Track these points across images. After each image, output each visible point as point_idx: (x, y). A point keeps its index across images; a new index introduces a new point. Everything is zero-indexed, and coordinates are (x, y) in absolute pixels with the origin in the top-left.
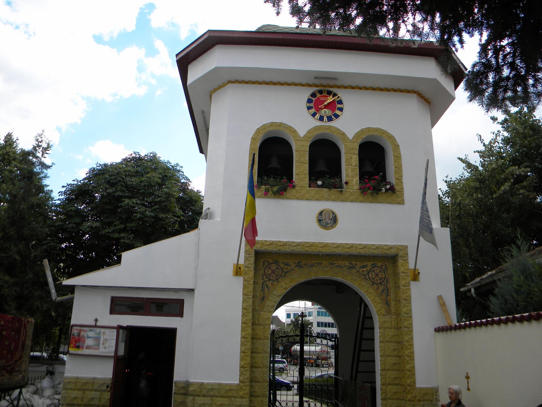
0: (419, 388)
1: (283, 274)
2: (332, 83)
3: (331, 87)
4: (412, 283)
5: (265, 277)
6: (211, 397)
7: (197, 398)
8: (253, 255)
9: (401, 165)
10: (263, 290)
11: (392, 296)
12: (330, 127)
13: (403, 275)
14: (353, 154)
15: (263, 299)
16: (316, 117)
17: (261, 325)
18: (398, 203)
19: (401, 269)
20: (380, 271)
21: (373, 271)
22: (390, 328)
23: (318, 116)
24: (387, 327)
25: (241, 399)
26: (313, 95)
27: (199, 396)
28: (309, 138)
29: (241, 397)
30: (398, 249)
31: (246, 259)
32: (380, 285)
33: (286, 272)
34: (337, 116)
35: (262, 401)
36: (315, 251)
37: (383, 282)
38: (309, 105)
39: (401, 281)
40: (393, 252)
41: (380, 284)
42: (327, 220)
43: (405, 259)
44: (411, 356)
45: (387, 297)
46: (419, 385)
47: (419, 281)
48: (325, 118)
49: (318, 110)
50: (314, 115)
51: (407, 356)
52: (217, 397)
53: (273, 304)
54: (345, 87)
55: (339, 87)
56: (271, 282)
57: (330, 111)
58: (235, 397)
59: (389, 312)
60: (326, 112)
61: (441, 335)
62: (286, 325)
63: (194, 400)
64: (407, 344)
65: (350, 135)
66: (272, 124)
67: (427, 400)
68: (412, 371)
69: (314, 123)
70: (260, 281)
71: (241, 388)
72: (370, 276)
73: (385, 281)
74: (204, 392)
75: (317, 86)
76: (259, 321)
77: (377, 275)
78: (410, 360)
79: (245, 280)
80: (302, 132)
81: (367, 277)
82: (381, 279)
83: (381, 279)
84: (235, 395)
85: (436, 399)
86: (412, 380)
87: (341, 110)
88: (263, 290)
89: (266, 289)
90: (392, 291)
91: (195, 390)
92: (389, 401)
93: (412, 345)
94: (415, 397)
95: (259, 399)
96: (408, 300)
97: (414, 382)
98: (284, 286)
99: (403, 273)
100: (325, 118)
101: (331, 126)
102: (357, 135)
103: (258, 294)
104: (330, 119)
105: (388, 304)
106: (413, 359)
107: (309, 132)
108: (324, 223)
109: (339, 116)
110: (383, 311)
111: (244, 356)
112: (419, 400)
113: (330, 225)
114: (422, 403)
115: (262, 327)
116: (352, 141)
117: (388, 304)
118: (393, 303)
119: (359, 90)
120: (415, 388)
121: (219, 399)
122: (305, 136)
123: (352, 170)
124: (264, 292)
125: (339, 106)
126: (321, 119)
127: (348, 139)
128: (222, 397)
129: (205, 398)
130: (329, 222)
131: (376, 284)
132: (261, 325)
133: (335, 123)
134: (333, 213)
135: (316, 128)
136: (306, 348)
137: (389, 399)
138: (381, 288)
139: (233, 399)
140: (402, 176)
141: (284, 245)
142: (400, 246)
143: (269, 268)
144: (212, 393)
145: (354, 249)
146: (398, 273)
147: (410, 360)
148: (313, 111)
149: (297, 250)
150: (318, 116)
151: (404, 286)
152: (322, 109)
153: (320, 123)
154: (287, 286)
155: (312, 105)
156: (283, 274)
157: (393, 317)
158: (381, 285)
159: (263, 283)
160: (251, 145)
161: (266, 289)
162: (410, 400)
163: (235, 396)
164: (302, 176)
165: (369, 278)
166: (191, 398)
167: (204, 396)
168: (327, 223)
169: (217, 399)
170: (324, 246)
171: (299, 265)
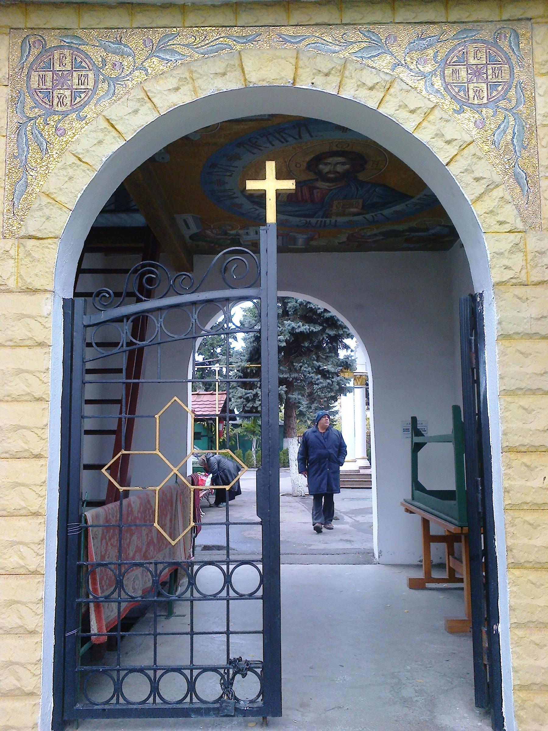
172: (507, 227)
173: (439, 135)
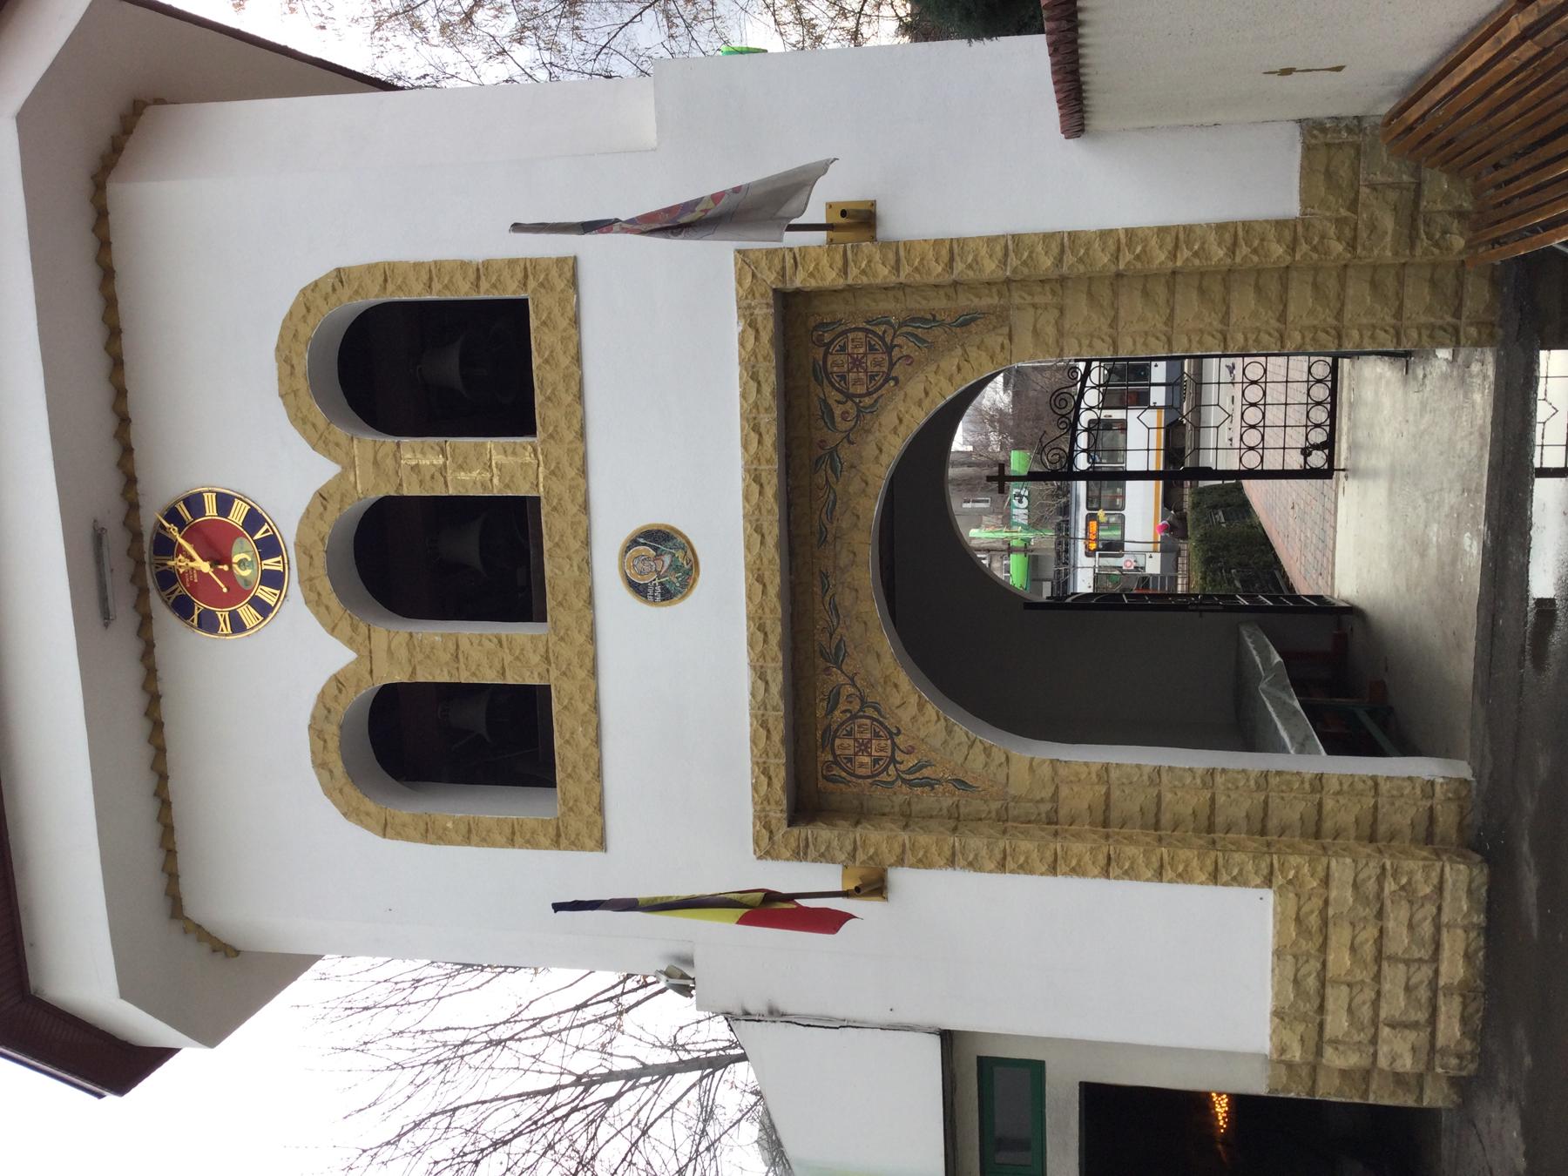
0: (1304, 203)
1: (870, 712)
2: (117, 539)
3: (137, 536)
4: (882, 232)
5: (884, 777)
6: (1323, 985)
7: (1329, 1032)
8: (807, 831)
10: (929, 783)
11: (939, 303)
13: (853, 271)
14: (397, 458)
15: (960, 783)
16: (271, 601)
17: (1055, 796)
18: (574, 282)
19: (831, 278)
20: (843, 348)
21: (843, 377)
22: (1062, 311)
23: (266, 594)
24: (1058, 325)
25: (1333, 884)
26: (183, 608)
27: (1321, 1026)
28: (354, 628)
29: (1326, 881)
30: (752, 292)
31: (825, 857)
32: (896, 353)
33: (862, 699)
34: (254, 520)
36: (779, 615)
37: (882, 339)
38: (225, 627)
39: (879, 281)
40: (765, 314)
41: (889, 349)
42: (663, 563)
43: (789, 262)
44: (1178, 236)
45: (942, 324)
46: (1289, 205)
47: (873, 204)
48: (271, 564)
49: (238, 592)
51: (1173, 256)
52: (1324, 964)
53: (978, 748)
54: (130, 481)
55: (133, 507)
56: (899, 756)
57: (236, 547)
58: (1326, 902)
59: (1001, 318)
60: (244, 560)
61: (1095, 122)
62: (1221, 1108)
63: (1335, 1042)
64: (1126, 257)
65: (323, 470)
66: (320, 765)
67: (1356, 174)
68: (1233, 233)
69: (294, 608)
70: (902, 794)
71: (1290, 882)
72: (861, 390)
73: (880, 330)
74: (1309, 1007)
75: (143, 593)
76: (1042, 800)
77: (857, 363)
78: (1189, 245)
79: (900, 862)
80: (337, 655)
81: (867, 401)
82: (872, 349)
83: (872, 349)
84: (1317, 903)
85: (1349, 130)
86: (1272, 234)
87: (225, 502)
88: (929, 783)
89: (926, 772)
90: (916, 304)
92: (1347, 316)
93: (1130, 233)
94: (1340, 222)
95: (1329, 804)
96: (952, 249)
97: (1280, 224)
98: (912, 709)
99: (845, 271)
100: (271, 564)
101: (299, 545)
102: (321, 444)
103: (947, 802)
104: (270, 547)
105: (967, 321)
106: (1188, 229)
107: (332, 630)
108: (674, 579)
109: (270, 609)
110: (995, 340)
111: (1174, 868)
113: (679, 554)
114: (1364, 191)
115: (1064, 791)
116: (349, 465)
117: (967, 321)
118: (966, 301)
119: (126, 340)
121: (1331, 957)
122: (350, 643)
123: (461, 468)
124: (939, 781)
125: (211, 510)
127: (341, 477)
128: (1324, 947)
129: (1330, 1005)
130: (667, 559)
131: (892, 365)
132: (1055, 796)
133: (286, 522)
134: (633, 542)
135: (315, 602)
136: (1081, 487)
137: (1339, 315)
138: (908, 348)
139: (1331, 912)
140: (463, 265)
141: (764, 724)
142: (739, 282)
143: (850, 760)
144: (1311, 983)
145: (764, 466)
147: (1189, 245)
148: (247, 614)
150: (266, 594)
152: (229, 577)
154: (914, 699)
155: (222, 614)
156: (870, 712)
157: (1016, 300)
158: (893, 347)
159: (904, 781)
161: (926, 772)
162: (1352, 245)
163: (1321, 903)
164: (508, 658)
165: (869, 394)
166: (1329, 1052)
167: (1321, 1009)
168: (675, 567)
169: (1330, 965)
170: (760, 579)
171: (836, 657)
172: (1006, 342)
173: (920, 404)
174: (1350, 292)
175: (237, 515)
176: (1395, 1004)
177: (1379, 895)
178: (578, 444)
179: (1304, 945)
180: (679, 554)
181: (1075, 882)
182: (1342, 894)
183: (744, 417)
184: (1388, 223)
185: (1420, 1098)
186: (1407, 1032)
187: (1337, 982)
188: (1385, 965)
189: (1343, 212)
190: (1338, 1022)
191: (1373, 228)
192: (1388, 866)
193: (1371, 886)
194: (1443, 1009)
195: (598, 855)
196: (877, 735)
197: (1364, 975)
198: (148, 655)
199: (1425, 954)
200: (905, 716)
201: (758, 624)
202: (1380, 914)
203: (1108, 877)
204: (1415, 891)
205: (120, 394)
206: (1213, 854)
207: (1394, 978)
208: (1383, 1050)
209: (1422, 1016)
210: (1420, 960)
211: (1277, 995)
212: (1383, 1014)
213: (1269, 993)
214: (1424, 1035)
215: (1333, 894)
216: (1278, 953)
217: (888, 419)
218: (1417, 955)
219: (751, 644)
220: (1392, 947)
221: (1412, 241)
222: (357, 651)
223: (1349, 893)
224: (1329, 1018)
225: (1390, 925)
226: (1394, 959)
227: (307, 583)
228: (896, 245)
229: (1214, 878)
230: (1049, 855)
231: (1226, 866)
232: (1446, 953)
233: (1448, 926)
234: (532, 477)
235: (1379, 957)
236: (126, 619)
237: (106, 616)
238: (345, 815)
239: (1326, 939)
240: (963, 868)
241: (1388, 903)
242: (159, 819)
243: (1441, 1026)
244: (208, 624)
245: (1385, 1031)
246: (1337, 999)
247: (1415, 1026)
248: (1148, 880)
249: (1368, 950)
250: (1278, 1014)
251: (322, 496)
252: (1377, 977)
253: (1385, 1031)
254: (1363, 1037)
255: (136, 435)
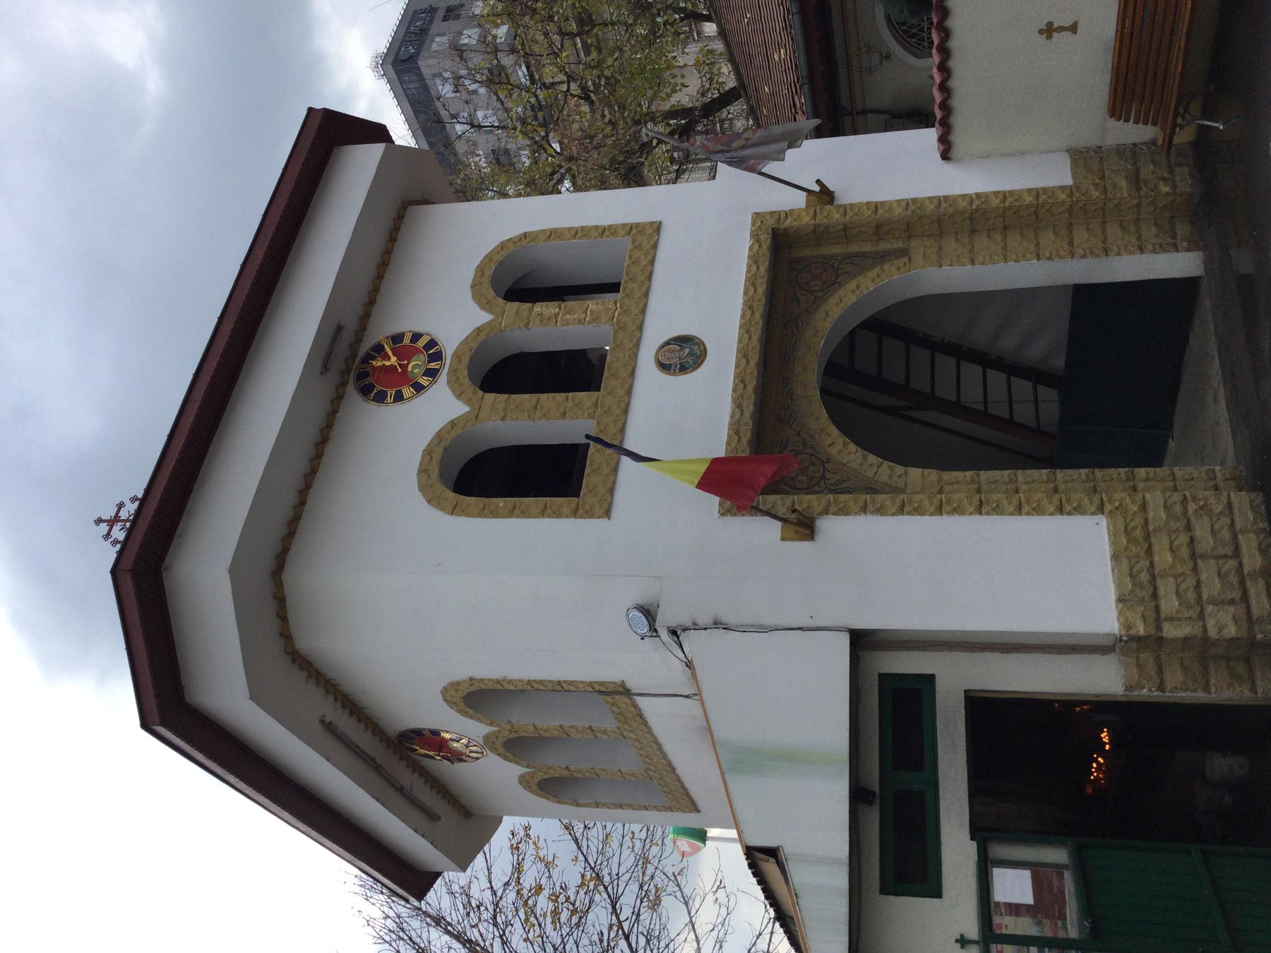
1: (810, 451)
2: (348, 336)
9: (570, 229)
12: (457, 355)
13: (819, 217)
27: (1157, 608)
29: (1144, 507)
35: (1146, 480)
40: (766, 239)
50: (419, 388)
52: (1152, 563)
56: (828, 475)
58: (1146, 521)
60: (416, 365)
61: (956, 151)
63: (1170, 619)
74: (1146, 594)
79: (826, 512)
81: (820, 294)
84: (1139, 521)
89: (845, 485)
91: (1143, 617)
94: (1096, 185)
97: (1063, 188)
98: (839, 446)
99: (815, 216)
100: (433, 365)
102: (485, 305)
104: (438, 356)
109: (437, 371)
112: (1102, 178)
113: (696, 348)
120: (1077, 186)
121: (1156, 558)
122: (468, 402)
125: (407, 341)
126: (432, 374)
129: (1161, 591)
131: (837, 277)
133: (449, 346)
134: (668, 343)
135: (453, 383)
142: (753, 225)
144: (1144, 577)
146: (816, 226)
148: (407, 391)
149: (752, 407)
150: (424, 381)
151: (845, 214)
153: (443, 377)
160: (468, 515)
161: (845, 485)
162: (1105, 191)
167: (1155, 595)
168: (691, 354)
169: (1156, 563)
170: (745, 356)
174: (1109, 232)
175: (421, 343)
176: (1213, 587)
177: (1185, 513)
178: (626, 398)
179: (1140, 593)
180: (696, 348)
181: (956, 519)
182: (1157, 515)
183: (734, 400)
184: (1123, 183)
185: (1253, 689)
186: (1227, 607)
187: (1164, 575)
188: (1199, 561)
189: (1097, 181)
190: (1169, 604)
191: (1115, 186)
192: (1188, 494)
193: (1178, 508)
194: (1244, 545)
195: (604, 521)
196: (813, 464)
197: (1186, 568)
198: (333, 412)
199: (1228, 551)
200: (833, 451)
201: (740, 379)
202: (1188, 527)
203: (980, 513)
204: (1211, 510)
205: (301, 503)
206: (1057, 496)
207: (1208, 571)
208: (1211, 623)
209: (1236, 595)
210: (1225, 556)
211: (1119, 586)
212: (1205, 597)
213: (1112, 586)
214: (1240, 610)
215: (1151, 515)
216: (1115, 557)
217: (833, 300)
218: (1222, 552)
219: (734, 390)
220: (1201, 548)
221: (1138, 189)
222: (472, 406)
223: (1163, 515)
224: (1162, 602)
225: (1198, 533)
226: (1202, 556)
227: (453, 372)
228: (845, 207)
229: (1060, 510)
230: (936, 502)
231: (1069, 501)
232: (1244, 550)
233: (1241, 531)
234: (611, 314)
235: (1193, 556)
236: (333, 377)
237: (325, 368)
238: (429, 501)
239: (1155, 589)
240: (872, 513)
241: (1193, 519)
242: (283, 539)
243: (1253, 602)
244: (380, 398)
245: (1210, 608)
246: (1166, 588)
247: (1232, 602)
248: (1010, 514)
249: (1184, 552)
250: (1120, 600)
251: (453, 424)
252: (1195, 569)
253: (1210, 609)
254: (1193, 613)
255: (303, 526)
